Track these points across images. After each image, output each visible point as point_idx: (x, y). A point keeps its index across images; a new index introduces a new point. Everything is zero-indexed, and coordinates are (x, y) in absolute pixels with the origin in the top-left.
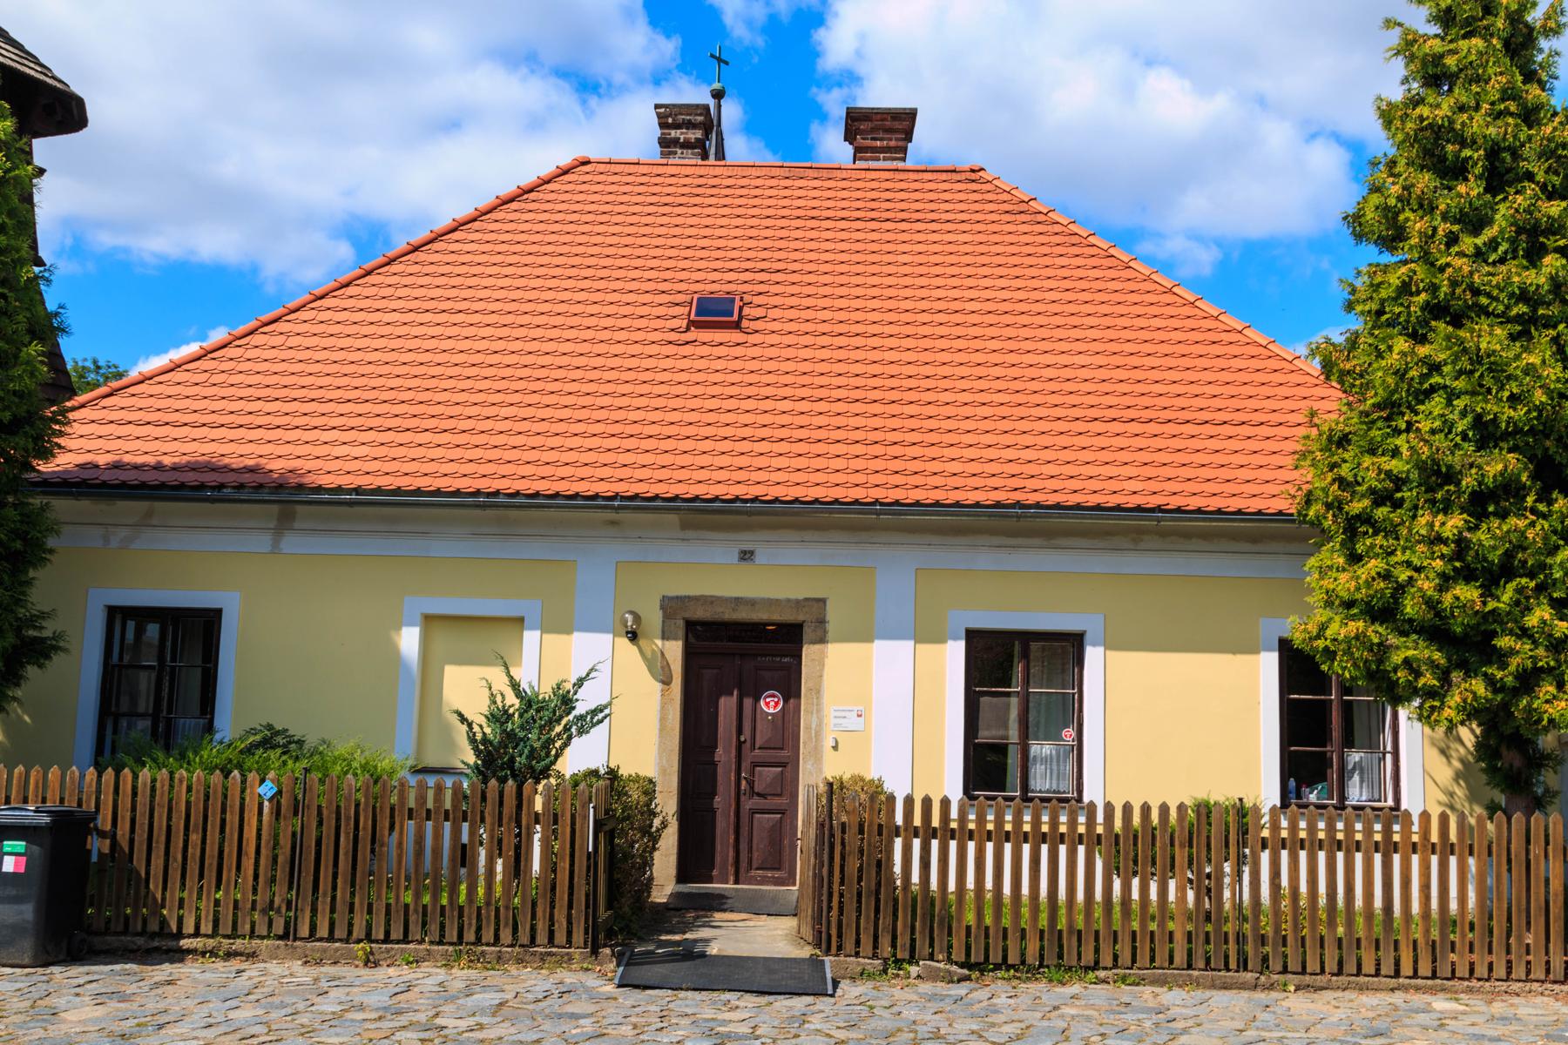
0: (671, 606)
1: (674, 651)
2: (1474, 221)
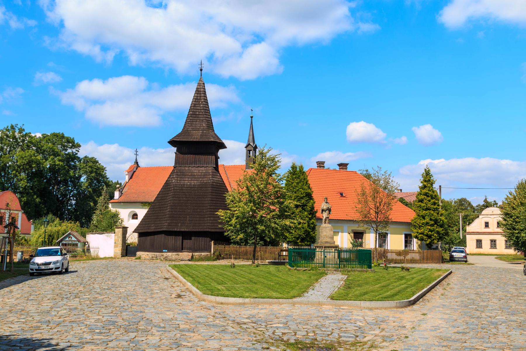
0: (352, 230)
1: (352, 235)
2: (429, 201)
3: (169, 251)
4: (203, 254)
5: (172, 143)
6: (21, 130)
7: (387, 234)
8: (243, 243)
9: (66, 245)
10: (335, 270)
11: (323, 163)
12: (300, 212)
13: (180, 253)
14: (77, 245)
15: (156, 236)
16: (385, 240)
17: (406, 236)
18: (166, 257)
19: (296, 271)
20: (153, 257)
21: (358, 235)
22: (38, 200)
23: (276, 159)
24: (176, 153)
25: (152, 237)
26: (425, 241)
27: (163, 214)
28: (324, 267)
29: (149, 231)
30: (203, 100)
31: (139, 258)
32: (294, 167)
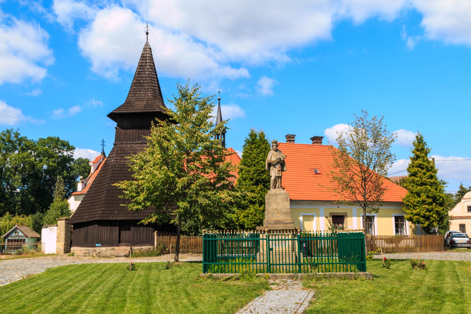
0: (330, 213)
1: (331, 219)
2: (425, 174)
3: (103, 245)
4: (144, 247)
5: (112, 116)
6: (17, 135)
7: (373, 217)
8: (192, 232)
9: (12, 241)
10: (292, 277)
11: (293, 136)
12: (261, 190)
13: (116, 248)
14: (24, 240)
15: (89, 227)
16: (371, 225)
17: (397, 219)
18: (99, 253)
19: (209, 281)
20: (85, 253)
21: (338, 219)
22: (32, 199)
23: (208, 103)
24: (116, 128)
25: (86, 228)
26: (422, 223)
27: (97, 201)
28: (269, 271)
29: (82, 221)
30: (148, 67)
31: (73, 255)
32: (253, 135)
